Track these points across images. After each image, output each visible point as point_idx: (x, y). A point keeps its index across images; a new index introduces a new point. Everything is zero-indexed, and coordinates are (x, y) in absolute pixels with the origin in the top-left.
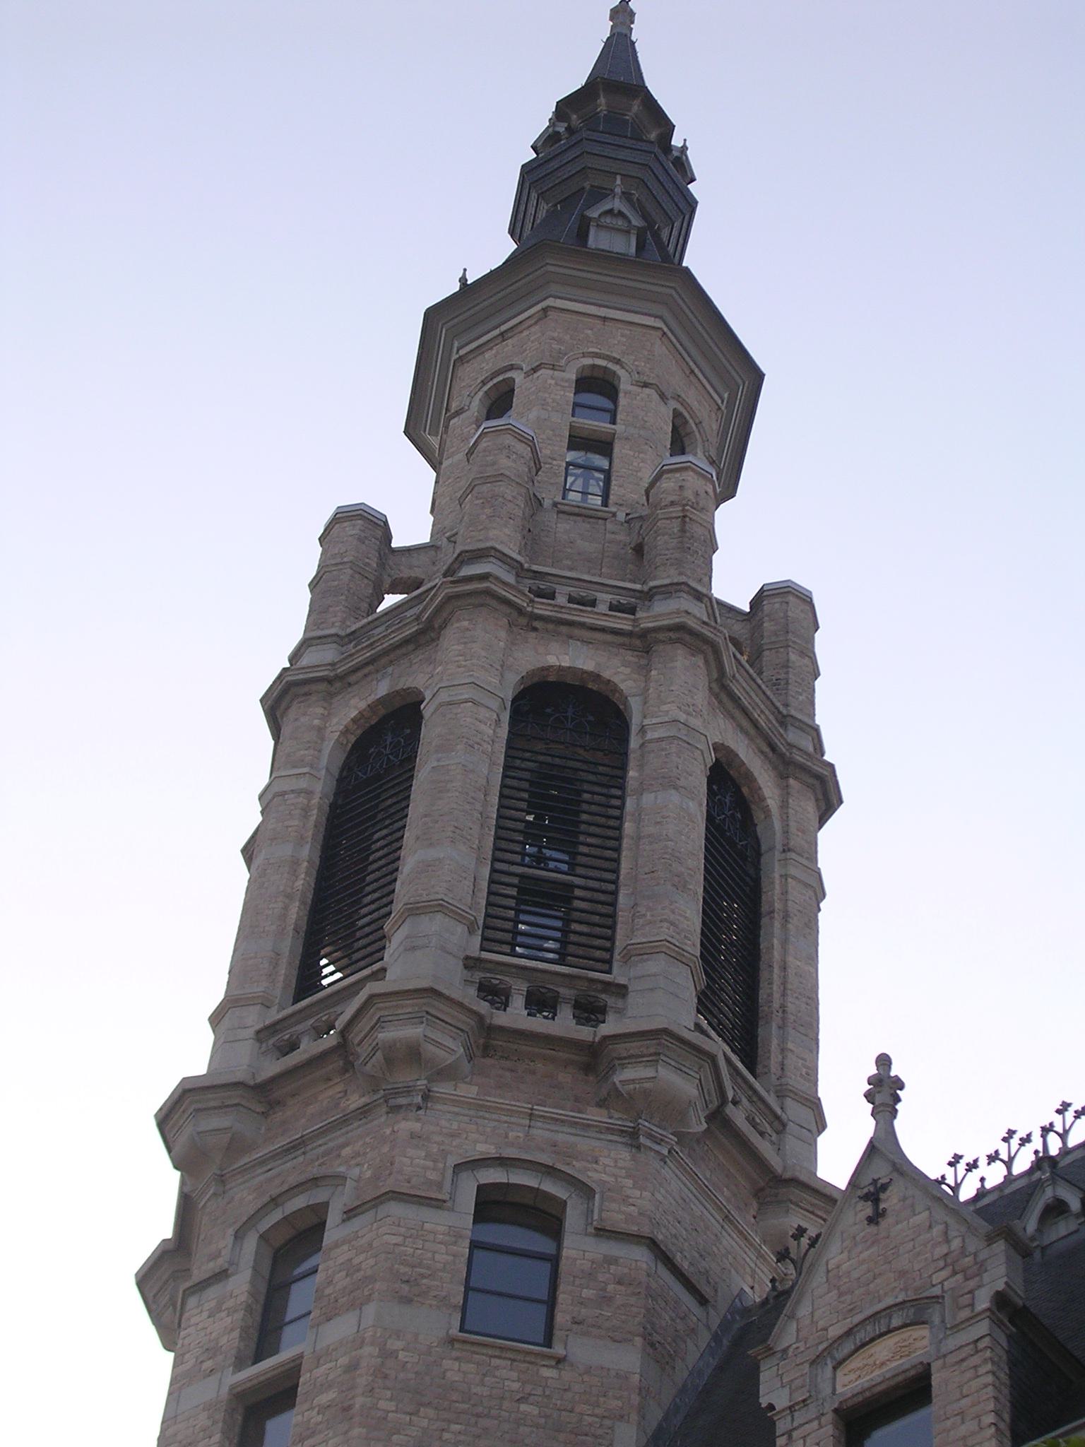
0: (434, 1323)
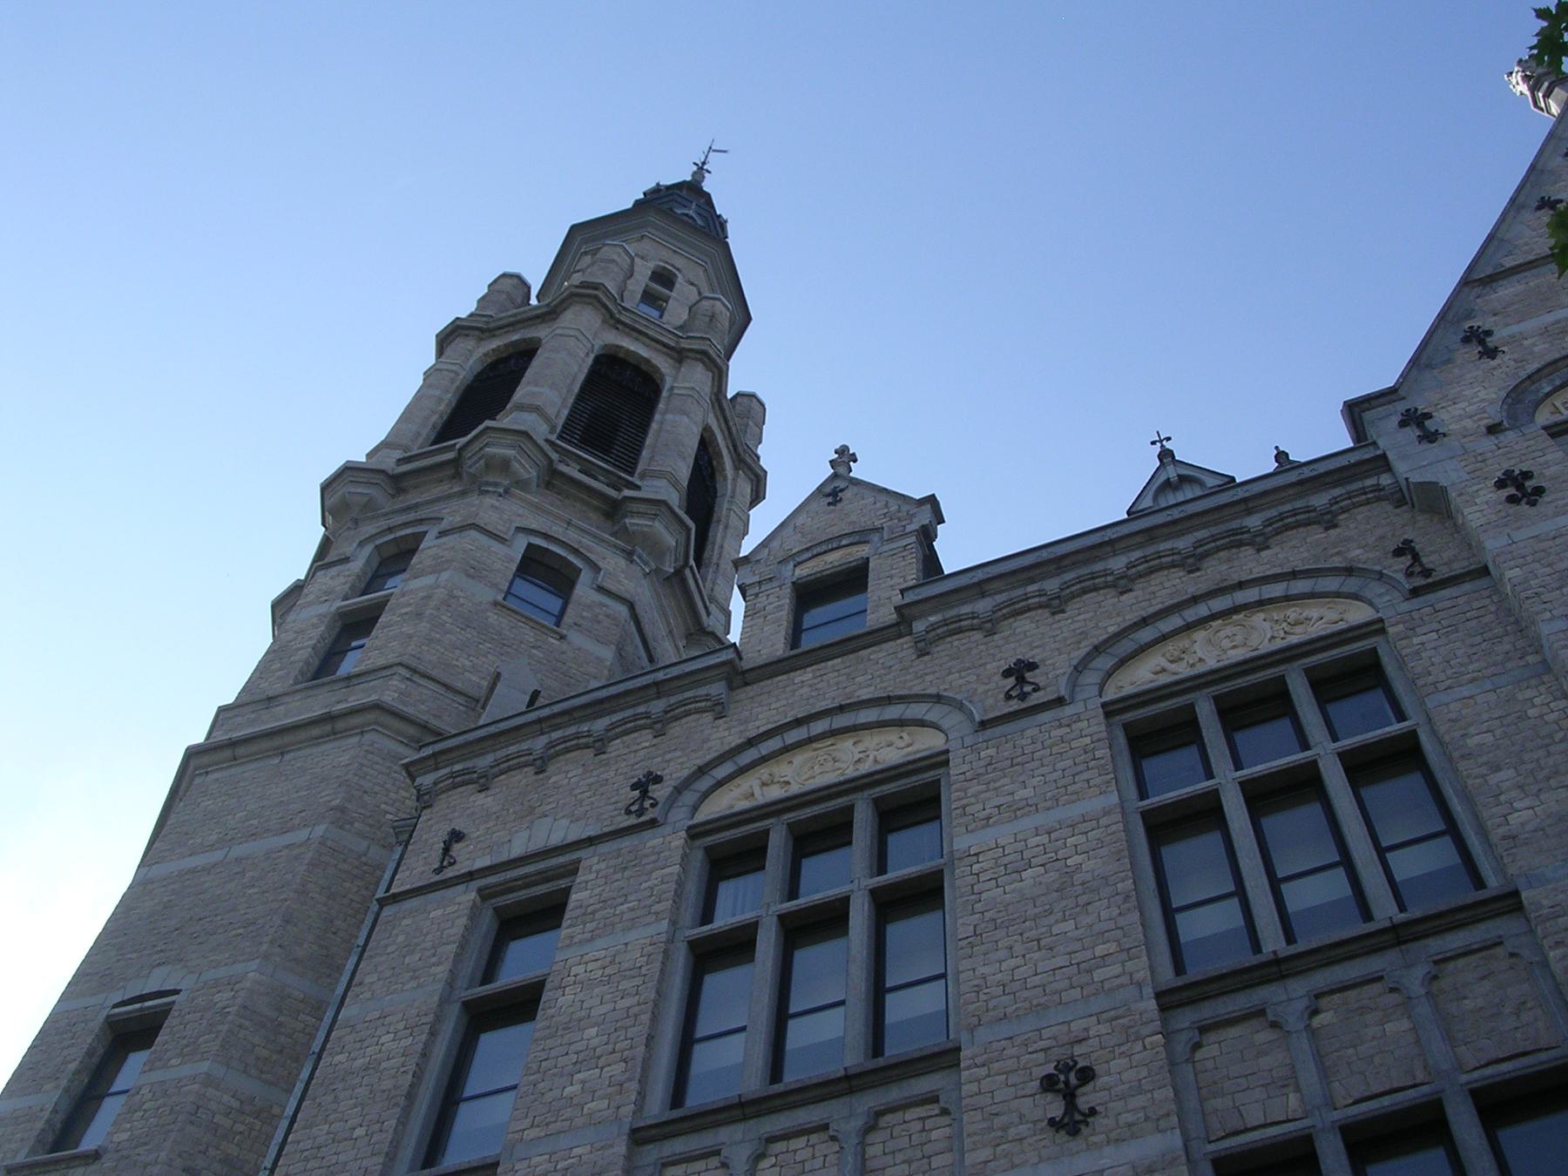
0: (485, 594)
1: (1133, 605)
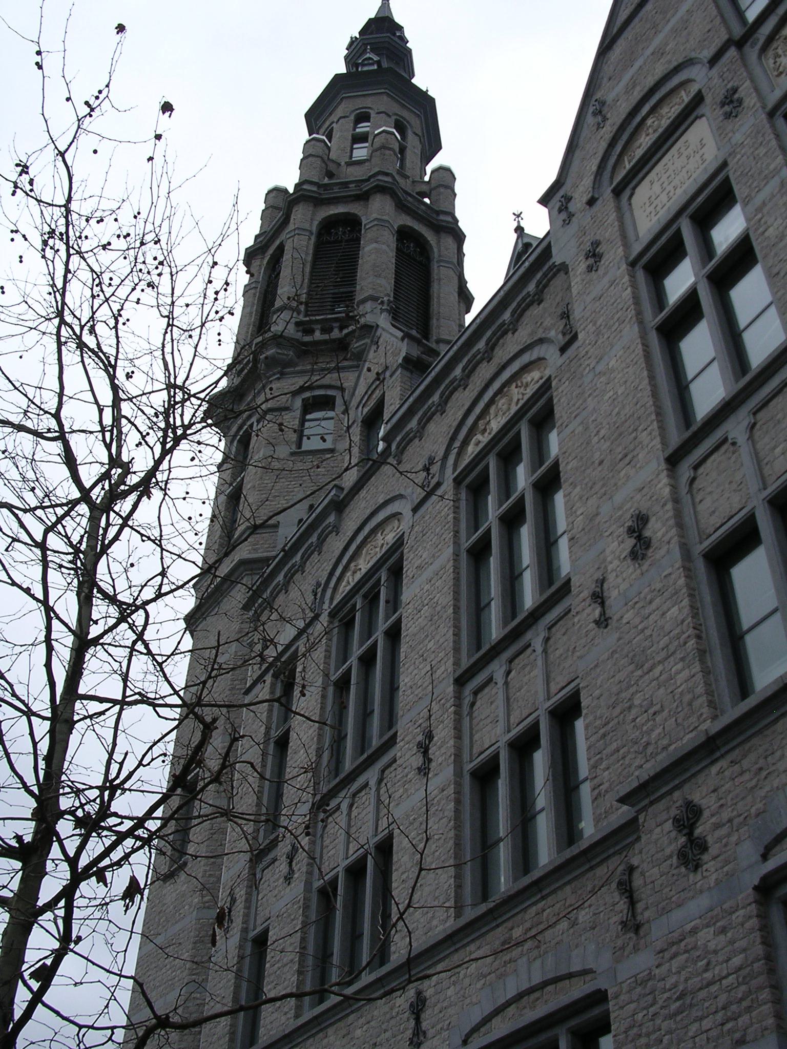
1: (454, 412)
